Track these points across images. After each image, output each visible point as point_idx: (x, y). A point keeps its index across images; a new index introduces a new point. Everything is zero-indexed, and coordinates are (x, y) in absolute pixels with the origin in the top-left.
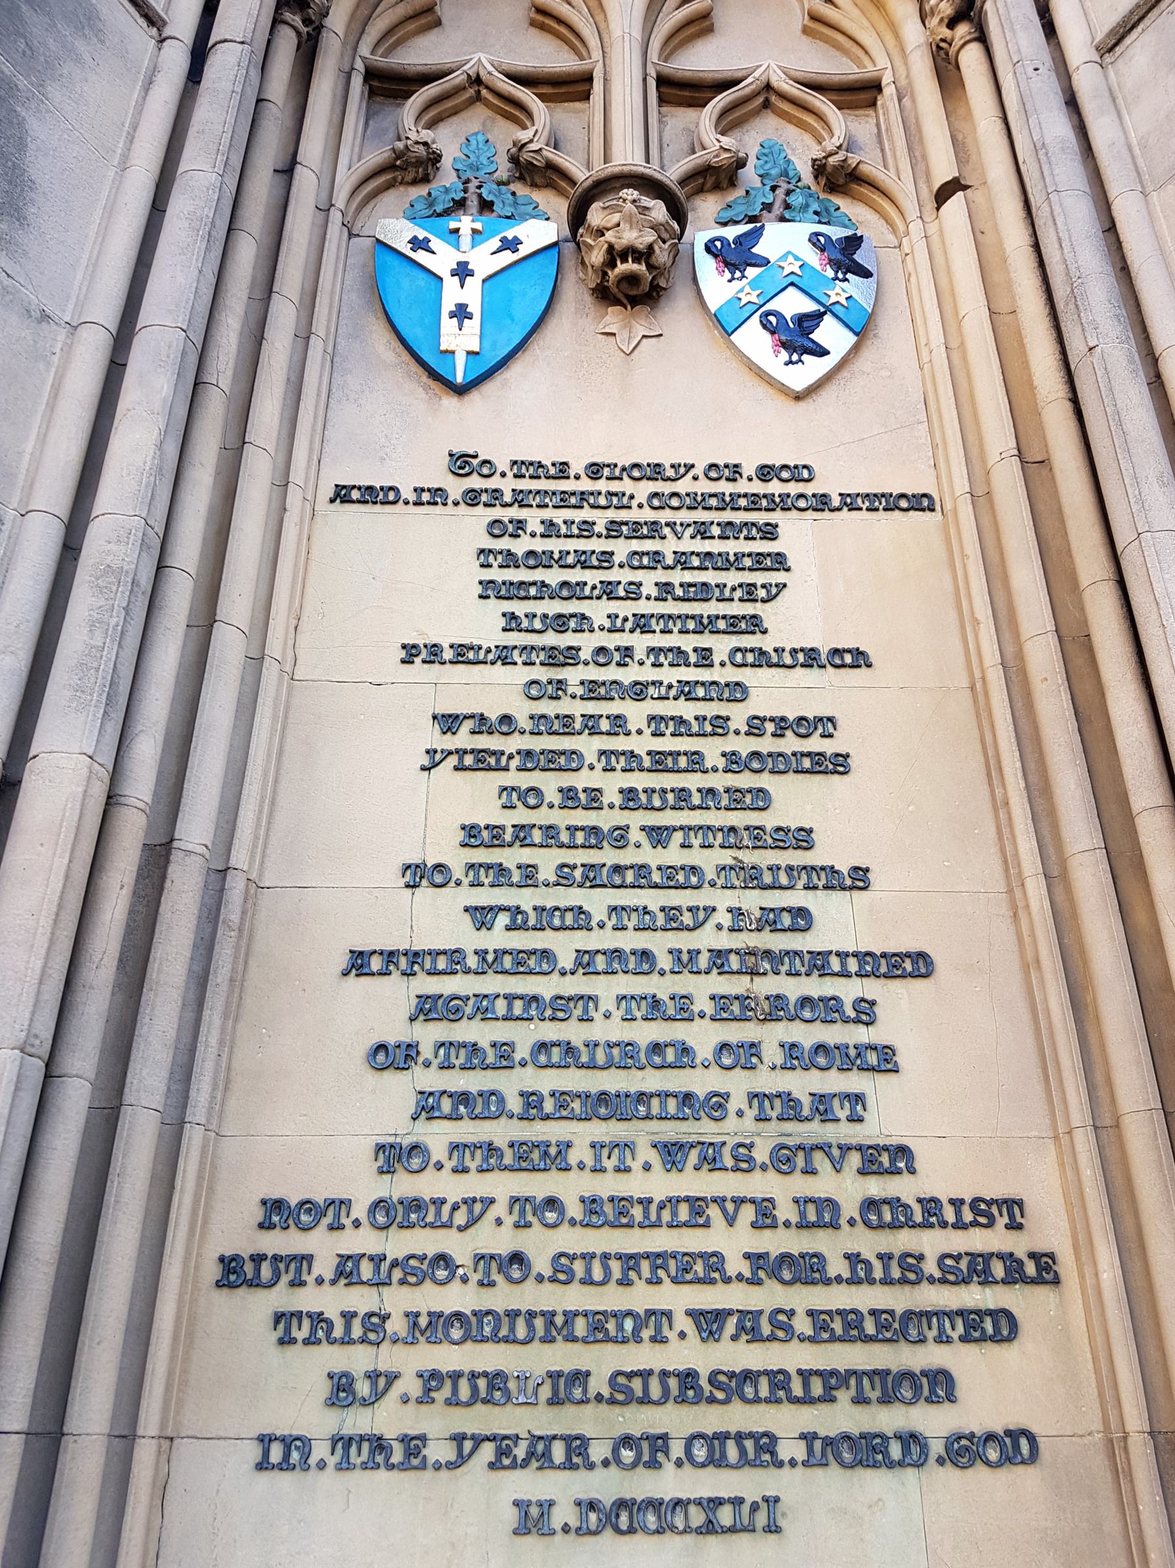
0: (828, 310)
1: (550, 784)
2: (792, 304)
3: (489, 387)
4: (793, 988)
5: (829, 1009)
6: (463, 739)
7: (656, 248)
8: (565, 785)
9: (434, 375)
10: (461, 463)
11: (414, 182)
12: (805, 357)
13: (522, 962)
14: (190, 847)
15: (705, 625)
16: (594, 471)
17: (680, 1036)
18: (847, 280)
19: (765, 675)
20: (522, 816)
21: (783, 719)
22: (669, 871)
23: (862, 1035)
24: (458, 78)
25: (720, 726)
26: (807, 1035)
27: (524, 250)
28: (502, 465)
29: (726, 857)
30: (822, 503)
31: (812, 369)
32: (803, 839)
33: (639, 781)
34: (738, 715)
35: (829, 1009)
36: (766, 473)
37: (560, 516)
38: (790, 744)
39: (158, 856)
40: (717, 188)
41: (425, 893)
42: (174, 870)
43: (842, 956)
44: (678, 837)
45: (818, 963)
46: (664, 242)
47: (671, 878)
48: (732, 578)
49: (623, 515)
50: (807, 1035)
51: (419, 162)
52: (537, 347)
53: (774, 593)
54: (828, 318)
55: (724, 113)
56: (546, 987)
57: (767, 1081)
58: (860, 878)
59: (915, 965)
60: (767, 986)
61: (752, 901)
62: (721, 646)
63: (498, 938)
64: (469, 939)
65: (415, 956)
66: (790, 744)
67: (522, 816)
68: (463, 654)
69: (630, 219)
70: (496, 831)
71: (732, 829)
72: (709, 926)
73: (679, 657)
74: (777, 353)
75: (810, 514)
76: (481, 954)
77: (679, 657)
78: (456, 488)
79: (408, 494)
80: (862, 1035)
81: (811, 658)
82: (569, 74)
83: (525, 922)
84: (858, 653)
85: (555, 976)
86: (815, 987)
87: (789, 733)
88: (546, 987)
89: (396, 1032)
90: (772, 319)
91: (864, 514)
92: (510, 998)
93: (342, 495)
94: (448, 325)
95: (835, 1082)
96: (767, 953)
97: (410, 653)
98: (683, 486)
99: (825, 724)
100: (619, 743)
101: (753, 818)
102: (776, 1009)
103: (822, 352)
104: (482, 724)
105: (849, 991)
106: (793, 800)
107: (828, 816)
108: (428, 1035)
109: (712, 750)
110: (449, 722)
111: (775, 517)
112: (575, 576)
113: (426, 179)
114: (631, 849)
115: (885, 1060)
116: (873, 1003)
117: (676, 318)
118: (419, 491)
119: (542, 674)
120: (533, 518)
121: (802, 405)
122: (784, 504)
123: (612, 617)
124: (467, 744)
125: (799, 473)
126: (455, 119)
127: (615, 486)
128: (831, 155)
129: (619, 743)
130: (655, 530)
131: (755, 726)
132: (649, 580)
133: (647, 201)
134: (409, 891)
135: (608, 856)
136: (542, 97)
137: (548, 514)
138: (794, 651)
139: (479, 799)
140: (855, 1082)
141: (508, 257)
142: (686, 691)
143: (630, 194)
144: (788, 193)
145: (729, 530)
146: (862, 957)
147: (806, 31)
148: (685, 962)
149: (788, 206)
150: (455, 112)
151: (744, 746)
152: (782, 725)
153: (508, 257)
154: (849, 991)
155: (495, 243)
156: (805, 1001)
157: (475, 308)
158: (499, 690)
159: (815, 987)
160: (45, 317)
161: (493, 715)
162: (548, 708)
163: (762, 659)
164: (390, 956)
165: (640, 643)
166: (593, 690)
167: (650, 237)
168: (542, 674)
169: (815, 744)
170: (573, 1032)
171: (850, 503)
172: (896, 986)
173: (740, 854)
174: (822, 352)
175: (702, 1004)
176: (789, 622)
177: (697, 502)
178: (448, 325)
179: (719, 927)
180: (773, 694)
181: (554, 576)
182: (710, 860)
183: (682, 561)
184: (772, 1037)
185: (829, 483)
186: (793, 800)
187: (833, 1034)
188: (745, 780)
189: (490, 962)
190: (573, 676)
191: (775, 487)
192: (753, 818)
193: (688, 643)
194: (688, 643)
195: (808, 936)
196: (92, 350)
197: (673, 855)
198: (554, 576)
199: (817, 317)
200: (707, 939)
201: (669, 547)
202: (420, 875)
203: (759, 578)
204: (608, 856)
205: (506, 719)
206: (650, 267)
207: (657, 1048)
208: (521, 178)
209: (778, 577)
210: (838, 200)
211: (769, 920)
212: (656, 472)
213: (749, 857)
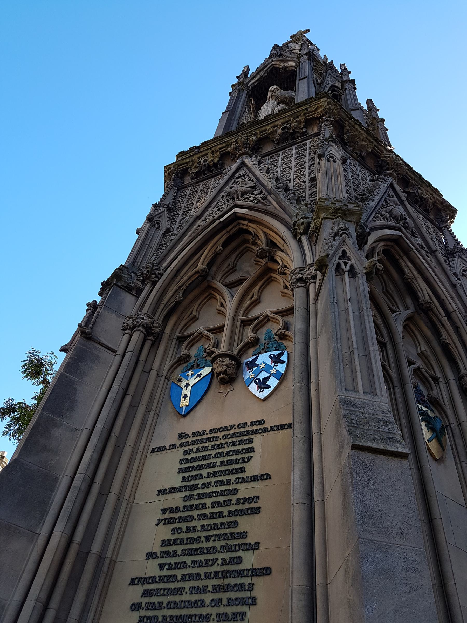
0: (272, 375)
1: (184, 526)
2: (263, 375)
3: (192, 413)
4: (232, 581)
5: (241, 587)
6: (167, 516)
7: (227, 370)
8: (187, 526)
9: (179, 414)
10: (181, 436)
11: (185, 363)
12: (265, 390)
13: (170, 579)
14: (93, 552)
15: (230, 472)
16: (211, 431)
17: (203, 598)
18: (277, 365)
19: (243, 485)
20: (176, 536)
21: (245, 498)
22: (208, 548)
23: (249, 594)
24: (196, 334)
25: (228, 503)
26: (233, 595)
27: (202, 376)
28: (190, 435)
29: (223, 543)
30: (265, 430)
31: (267, 392)
32: (244, 535)
33: (206, 522)
34: (234, 498)
35: (241, 587)
36: (252, 424)
37: (200, 446)
38: (247, 506)
39: (83, 556)
40: (253, 346)
41: (151, 561)
42: (89, 558)
43: (248, 570)
44: (213, 538)
45: (241, 573)
46: (230, 368)
47: (210, 551)
48: (239, 457)
49: (216, 443)
50: (233, 595)
51: (184, 358)
52: (205, 401)
53: (250, 458)
54: (271, 377)
55: (255, 327)
56: (172, 586)
57: (222, 610)
58: (257, 546)
59: (265, 572)
60: (227, 581)
61: (228, 555)
62: (233, 478)
63: (165, 572)
64: (157, 573)
65: (145, 579)
66: (247, 506)
67: (176, 536)
68: (172, 490)
69: (219, 365)
70: (169, 541)
71: (226, 534)
72: (216, 564)
73: (222, 483)
74: (258, 390)
75: (262, 434)
76: (160, 577)
77: (222, 483)
78: (178, 443)
79: (168, 447)
80: (249, 594)
81: (255, 478)
82: (220, 326)
83: (172, 567)
84: (268, 475)
85: (176, 582)
86: (239, 581)
87: (246, 503)
88: (172, 586)
89: (137, 600)
90: (257, 381)
91: (276, 432)
92: (165, 589)
93: (153, 451)
94: (182, 399)
95: (240, 609)
96: (228, 571)
97: (159, 491)
98: (231, 432)
99: (255, 499)
100: (203, 512)
101: (232, 530)
102: (228, 588)
103: (269, 387)
104: (172, 510)
105: (247, 581)
106: (245, 524)
107: (252, 527)
108: (145, 600)
109: (225, 510)
110: (164, 511)
111: (254, 436)
112: (200, 463)
113: (187, 361)
114: (201, 543)
115: (253, 601)
116: (253, 584)
117: (238, 386)
118: (170, 446)
119: (188, 493)
120: (194, 448)
121: (265, 402)
122: (255, 432)
123: (208, 473)
124: (168, 517)
125: (261, 422)
126: (197, 343)
127: (215, 435)
128: (277, 332)
129: (203, 512)
130: (222, 446)
131: (238, 502)
132: (218, 461)
133: (224, 360)
134: (147, 561)
135: (195, 546)
136: (212, 333)
137: (198, 446)
138: (251, 477)
139: (166, 533)
140: (245, 609)
141: (199, 379)
142: (222, 493)
143: (219, 359)
144: (268, 344)
145: (241, 442)
146: (253, 570)
147: (282, 296)
148: (208, 576)
149: (268, 348)
150: (197, 341)
151: (233, 508)
152: (245, 500)
153: (199, 379)
154: (247, 581)
155: (196, 376)
156: (235, 585)
157: (189, 395)
158: (176, 500)
159: (239, 581)
160: (76, 430)
161: (174, 507)
162: (188, 503)
163: (243, 480)
164: (140, 579)
165: (213, 480)
166: (200, 496)
167: (225, 368)
168: (188, 493)
169: (253, 505)
170: (177, 598)
171: (272, 429)
172: (261, 579)
173: (227, 542)
174: (269, 387)
175: (210, 588)
176: (254, 468)
177: (234, 435)
178: (182, 399)
179: (218, 565)
180: (245, 490)
181: (195, 464)
182: (218, 544)
183: (228, 454)
184: (225, 596)
185: (268, 425)
186: (245, 524)
187: (240, 595)
188: (232, 519)
189: (162, 579)
190: (195, 493)
191: (255, 427)
192: (232, 530)
193: (224, 478)
194: (224, 478)
195: (241, 565)
196: (85, 434)
197: (211, 544)
198: (195, 464)
199: (269, 377)
200: (215, 568)
201: (224, 450)
202: (151, 556)
203: (246, 455)
204: (195, 546)
205: (177, 508)
206: (227, 375)
207: (196, 602)
208: (208, 355)
209: (251, 454)
210: (283, 342)
211: (231, 561)
212: (226, 429)
213: (229, 542)
